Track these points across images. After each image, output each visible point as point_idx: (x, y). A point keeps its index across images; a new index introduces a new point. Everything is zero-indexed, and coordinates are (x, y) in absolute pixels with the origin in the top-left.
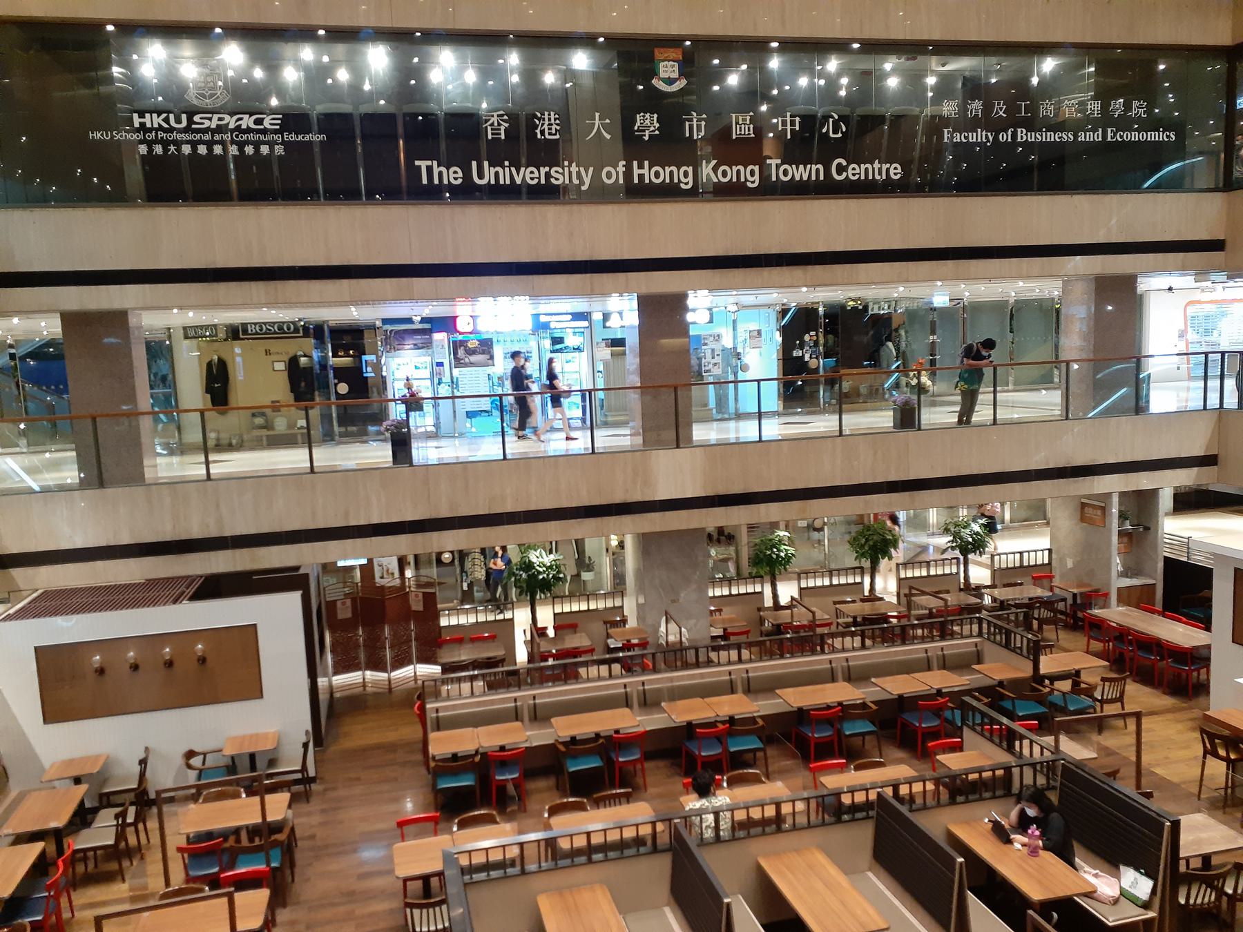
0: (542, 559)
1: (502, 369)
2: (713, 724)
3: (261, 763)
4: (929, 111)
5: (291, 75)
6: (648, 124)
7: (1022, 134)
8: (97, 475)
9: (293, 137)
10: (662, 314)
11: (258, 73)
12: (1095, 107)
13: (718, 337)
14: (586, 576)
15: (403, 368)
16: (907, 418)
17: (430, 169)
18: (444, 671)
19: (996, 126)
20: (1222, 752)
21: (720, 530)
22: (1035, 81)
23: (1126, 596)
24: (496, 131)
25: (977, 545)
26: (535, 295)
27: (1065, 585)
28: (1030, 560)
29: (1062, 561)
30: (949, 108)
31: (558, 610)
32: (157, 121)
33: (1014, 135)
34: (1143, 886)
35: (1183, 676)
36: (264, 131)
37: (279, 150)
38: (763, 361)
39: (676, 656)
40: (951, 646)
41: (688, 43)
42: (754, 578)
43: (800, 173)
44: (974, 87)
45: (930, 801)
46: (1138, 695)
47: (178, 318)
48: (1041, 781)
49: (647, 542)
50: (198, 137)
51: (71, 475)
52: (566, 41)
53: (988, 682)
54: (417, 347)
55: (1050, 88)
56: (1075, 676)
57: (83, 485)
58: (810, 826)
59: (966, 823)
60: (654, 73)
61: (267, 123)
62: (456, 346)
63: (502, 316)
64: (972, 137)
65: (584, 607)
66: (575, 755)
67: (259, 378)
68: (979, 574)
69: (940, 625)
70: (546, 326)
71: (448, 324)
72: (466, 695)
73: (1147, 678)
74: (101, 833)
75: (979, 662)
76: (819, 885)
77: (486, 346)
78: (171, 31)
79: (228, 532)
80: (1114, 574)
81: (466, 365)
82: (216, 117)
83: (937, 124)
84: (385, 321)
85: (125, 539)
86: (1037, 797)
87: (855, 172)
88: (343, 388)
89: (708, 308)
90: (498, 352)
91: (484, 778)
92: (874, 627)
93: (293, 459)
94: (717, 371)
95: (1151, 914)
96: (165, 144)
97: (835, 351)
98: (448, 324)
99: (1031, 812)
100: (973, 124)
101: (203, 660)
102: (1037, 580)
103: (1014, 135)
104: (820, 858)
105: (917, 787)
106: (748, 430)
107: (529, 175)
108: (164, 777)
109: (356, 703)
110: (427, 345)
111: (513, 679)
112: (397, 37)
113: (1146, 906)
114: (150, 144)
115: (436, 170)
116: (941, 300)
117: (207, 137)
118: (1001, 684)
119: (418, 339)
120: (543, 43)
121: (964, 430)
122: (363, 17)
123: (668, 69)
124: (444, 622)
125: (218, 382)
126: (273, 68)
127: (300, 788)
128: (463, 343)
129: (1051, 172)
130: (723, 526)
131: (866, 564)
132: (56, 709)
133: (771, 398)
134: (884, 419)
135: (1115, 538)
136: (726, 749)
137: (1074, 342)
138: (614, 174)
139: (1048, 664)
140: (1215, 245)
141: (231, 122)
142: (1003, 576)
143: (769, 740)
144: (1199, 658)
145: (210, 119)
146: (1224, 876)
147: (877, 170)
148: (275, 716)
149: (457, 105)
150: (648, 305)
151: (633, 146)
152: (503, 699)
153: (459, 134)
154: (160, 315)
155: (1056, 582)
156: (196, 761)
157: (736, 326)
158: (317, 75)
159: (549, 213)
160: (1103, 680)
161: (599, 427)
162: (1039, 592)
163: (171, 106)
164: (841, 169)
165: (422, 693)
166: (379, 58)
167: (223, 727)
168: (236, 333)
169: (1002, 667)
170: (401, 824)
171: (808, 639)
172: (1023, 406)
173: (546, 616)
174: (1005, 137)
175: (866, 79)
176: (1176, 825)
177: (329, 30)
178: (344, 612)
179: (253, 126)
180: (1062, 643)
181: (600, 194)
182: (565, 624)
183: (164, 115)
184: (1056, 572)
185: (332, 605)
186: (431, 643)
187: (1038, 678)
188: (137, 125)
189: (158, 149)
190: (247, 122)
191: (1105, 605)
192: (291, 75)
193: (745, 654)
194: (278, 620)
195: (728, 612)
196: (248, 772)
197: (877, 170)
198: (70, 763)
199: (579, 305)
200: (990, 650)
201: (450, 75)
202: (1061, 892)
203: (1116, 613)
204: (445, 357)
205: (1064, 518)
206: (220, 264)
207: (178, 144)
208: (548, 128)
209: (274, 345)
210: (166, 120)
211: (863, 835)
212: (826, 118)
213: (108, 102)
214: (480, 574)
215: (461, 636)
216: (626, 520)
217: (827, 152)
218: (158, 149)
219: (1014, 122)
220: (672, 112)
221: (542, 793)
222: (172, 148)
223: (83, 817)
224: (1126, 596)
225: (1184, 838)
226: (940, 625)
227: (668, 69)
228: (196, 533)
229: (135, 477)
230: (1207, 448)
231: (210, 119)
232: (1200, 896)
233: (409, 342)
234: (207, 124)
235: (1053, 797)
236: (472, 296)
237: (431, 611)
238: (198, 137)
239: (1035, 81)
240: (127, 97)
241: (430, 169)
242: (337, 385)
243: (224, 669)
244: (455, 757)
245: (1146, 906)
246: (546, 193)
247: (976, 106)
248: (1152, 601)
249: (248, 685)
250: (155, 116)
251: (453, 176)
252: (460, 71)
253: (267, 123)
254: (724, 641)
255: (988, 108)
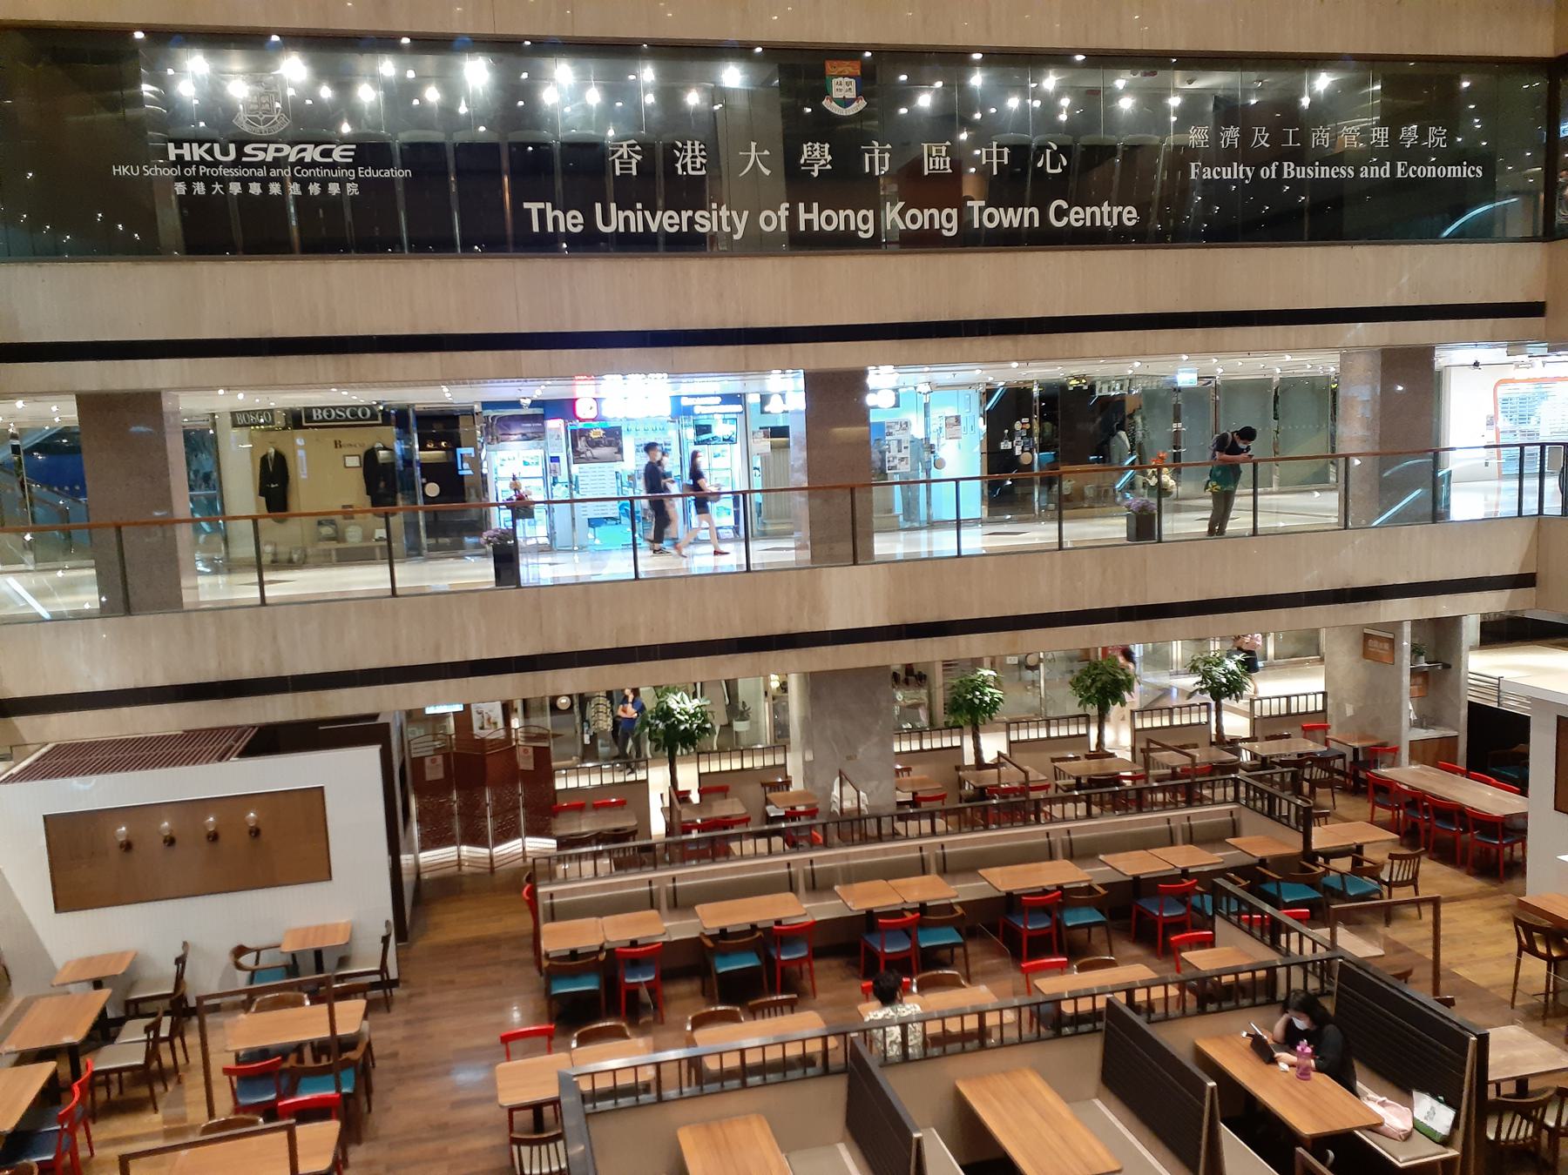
0: (683, 704)
1: (634, 465)
2: (899, 913)
3: (329, 962)
4: (1171, 139)
5: (367, 95)
6: (818, 156)
7: (1289, 170)
8: (122, 598)
9: (370, 173)
10: (836, 396)
11: (326, 93)
12: (1381, 135)
13: (906, 425)
14: (739, 726)
15: (509, 464)
16: (1144, 527)
17: (542, 213)
18: (560, 846)
19: (1256, 159)
20: (1542, 949)
21: (909, 669)
22: (1305, 102)
23: (1420, 752)
24: (626, 165)
25: (1233, 688)
26: (674, 372)
27: (1343, 738)
28: (1299, 706)
29: (1340, 707)
30: (1197, 136)
31: (704, 769)
32: (198, 152)
33: (1279, 170)
34: (1441, 1118)
35: (1492, 852)
36: (334, 166)
37: (352, 189)
38: (962, 455)
39: (853, 827)
40: (1200, 815)
41: (868, 54)
42: (951, 728)
43: (1009, 218)
44: (1228, 110)
45: (1173, 1010)
46: (1436, 877)
47: (225, 401)
48: (1313, 984)
49: (816, 684)
50: (250, 172)
51: (90, 599)
52: (714, 51)
53: (1247, 860)
54: (526, 438)
55: (1324, 111)
56: (1356, 852)
57: (105, 611)
58: (1021, 1041)
59: (1219, 1037)
60: (825, 92)
61: (337, 155)
62: (576, 436)
63: (633, 398)
64: (1227, 173)
65: (736, 765)
66: (725, 952)
67: (327, 477)
68: (1236, 724)
69: (1186, 788)
70: (688, 411)
71: (565, 408)
72: (588, 877)
73: (1447, 854)
74: (128, 1051)
75: (1235, 834)
76: (1033, 1116)
77: (613, 437)
78: (216, 39)
79: (287, 671)
80: (1405, 723)
81: (588, 460)
82: (272, 147)
83: (1182, 157)
84: (486, 405)
85: (158, 680)
86: (1308, 1005)
87: (1078, 217)
88: (433, 489)
89: (893, 388)
90: (628, 443)
91: (611, 981)
92: (1103, 790)
93: (369, 578)
94: (904, 468)
95: (1452, 1153)
96: (209, 181)
97: (1053, 443)
98: (565, 408)
99: (1301, 1024)
100: (1227, 157)
101: (255, 832)
102: (1308, 732)
103: (1279, 170)
104: (1035, 1082)
105: (1157, 993)
106: (944, 543)
107: (667, 221)
108: (206, 980)
109: (449, 886)
110: (539, 435)
111: (648, 856)
112: (501, 46)
113: (1446, 1142)
114: (189, 182)
115: (550, 215)
116: (1186, 378)
117: (261, 173)
118: (1262, 862)
119: (528, 427)
120: (685, 54)
121: (1217, 543)
122: (458, 21)
123: (843, 87)
124: (560, 784)
125: (275, 481)
126: (344, 85)
127: (379, 993)
128: (583, 433)
129: (1325, 217)
130: (912, 663)
131: (1093, 710)
132: (71, 893)
133: (973, 501)
134: (1115, 528)
135: (1406, 679)
136: (915, 945)
137: (1354, 431)
138: (775, 219)
139: (1322, 837)
140: (1533, 310)
141: (292, 154)
142: (1266, 726)
143: (970, 933)
144: (1513, 829)
145: (265, 150)
146: (1544, 1105)
147: (1106, 214)
148: (348, 903)
149: (576, 133)
150: (817, 384)
151: (798, 184)
152: (635, 881)
153: (578, 169)
154: (202, 397)
155: (1333, 733)
156: (248, 960)
157: (929, 411)
158: (400, 94)
159: (693, 269)
160: (1392, 857)
161: (755, 539)
162: (1311, 746)
163: (215, 134)
164: (1060, 214)
165: (532, 873)
166: (478, 74)
167: (282, 916)
168: (297, 419)
169: (1264, 841)
170: (506, 1039)
171: (1019, 806)
172: (1291, 511)
173: (688, 777)
174: (1268, 173)
175: (1093, 100)
176: (1483, 1040)
177: (415, 38)
178: (434, 772)
179: (319, 159)
180: (1340, 810)
181: (757, 245)
182: (712, 787)
183: (207, 146)
184: (1333, 721)
185: (419, 763)
186: (544, 811)
187: (1309, 855)
188: (172, 158)
189: (200, 188)
190: (312, 153)
191: (1395, 763)
192: (367, 95)
193: (940, 824)
194: (350, 782)
195: (918, 772)
196: (313, 974)
197: (1106, 214)
198: (88, 961)
199: (731, 384)
200: (1248, 819)
201: (568, 95)
202: (1338, 1125)
203: (1407, 773)
204: (562, 450)
205: (1342, 653)
206: (278, 332)
207: (224, 181)
208: (691, 161)
209: (346, 436)
210: (210, 152)
211: (1088, 1052)
212: (1042, 149)
213: (136, 129)
214: (606, 724)
215: (581, 802)
216: (790, 655)
217: (1043, 191)
218: (200, 188)
219: (1279, 154)
220: (848, 141)
221: (684, 999)
222: (217, 186)
223: (104, 1030)
224: (1420, 752)
225: (1494, 1057)
226: (1186, 788)
227: (843, 87)
228: (247, 672)
229: (170, 601)
230: (1523, 565)
231: (265, 150)
232: (1514, 1130)
233: (517, 431)
234: (261, 156)
235: (1329, 1005)
236: (595, 373)
237: (543, 770)
238: (250, 172)
239: (1305, 102)
240: (160, 122)
241: (542, 213)
242: (425, 485)
243: (283, 843)
244: (574, 954)
245: (1446, 1142)
246: (689, 243)
247: (1232, 134)
248: (1453, 757)
249: (312, 863)
250: (195, 146)
251: (572, 222)
252: (581, 89)
253: (337, 155)
254: (914, 808)
255: (1246, 136)
